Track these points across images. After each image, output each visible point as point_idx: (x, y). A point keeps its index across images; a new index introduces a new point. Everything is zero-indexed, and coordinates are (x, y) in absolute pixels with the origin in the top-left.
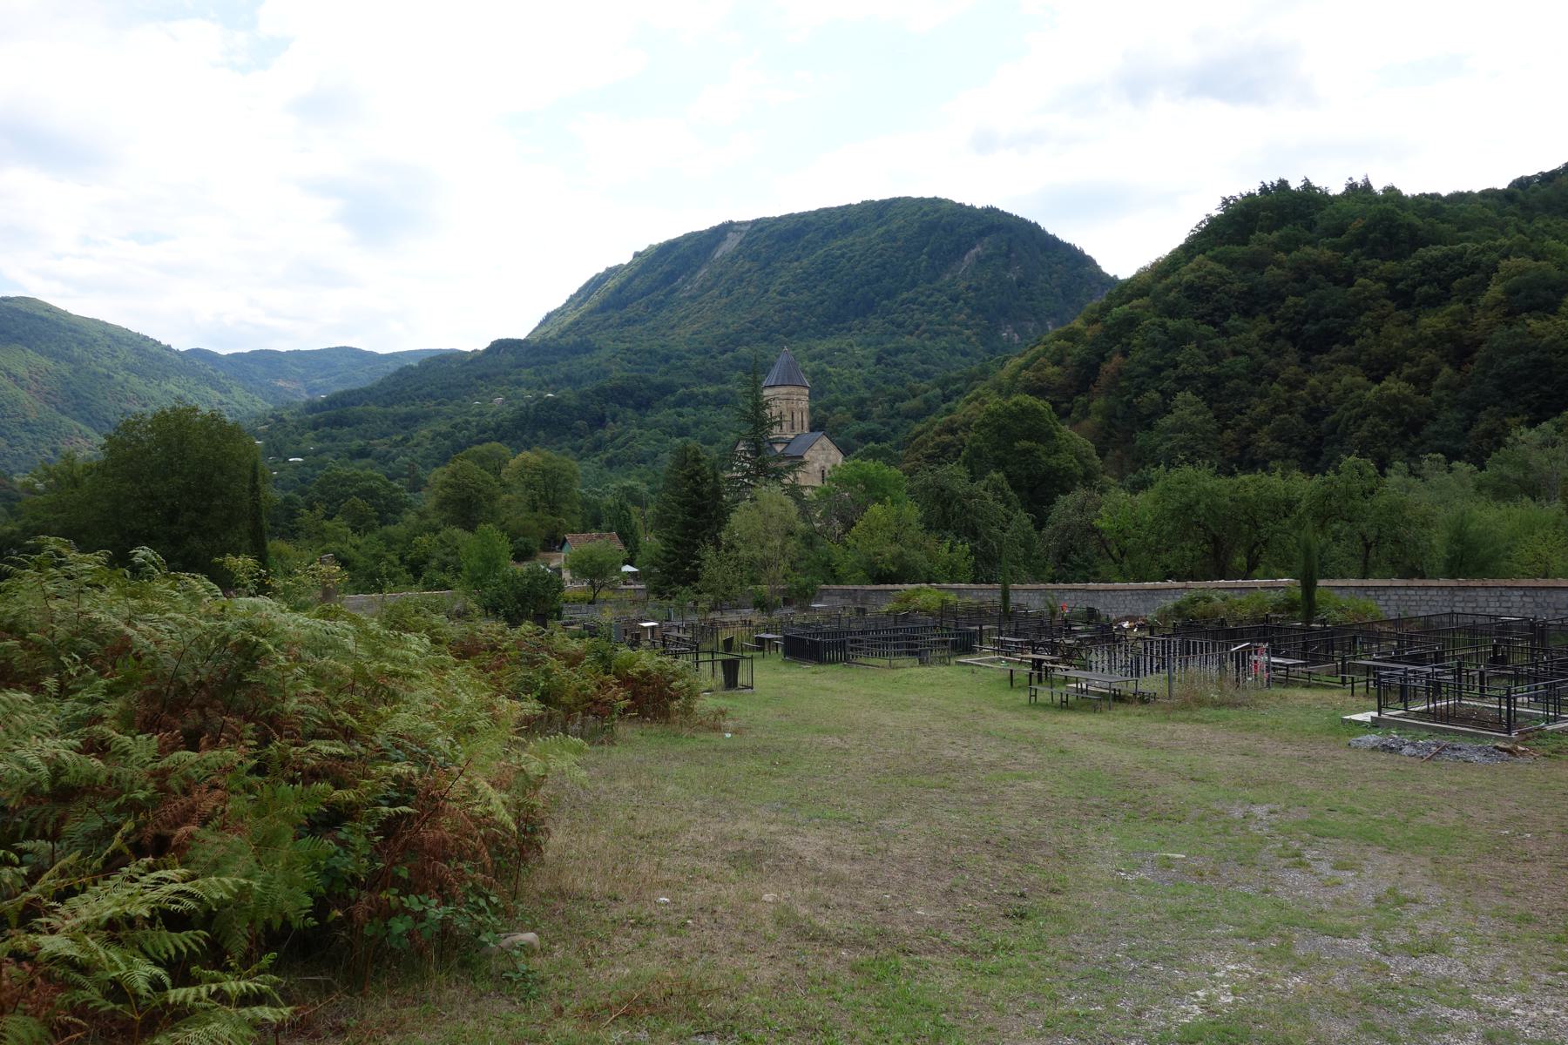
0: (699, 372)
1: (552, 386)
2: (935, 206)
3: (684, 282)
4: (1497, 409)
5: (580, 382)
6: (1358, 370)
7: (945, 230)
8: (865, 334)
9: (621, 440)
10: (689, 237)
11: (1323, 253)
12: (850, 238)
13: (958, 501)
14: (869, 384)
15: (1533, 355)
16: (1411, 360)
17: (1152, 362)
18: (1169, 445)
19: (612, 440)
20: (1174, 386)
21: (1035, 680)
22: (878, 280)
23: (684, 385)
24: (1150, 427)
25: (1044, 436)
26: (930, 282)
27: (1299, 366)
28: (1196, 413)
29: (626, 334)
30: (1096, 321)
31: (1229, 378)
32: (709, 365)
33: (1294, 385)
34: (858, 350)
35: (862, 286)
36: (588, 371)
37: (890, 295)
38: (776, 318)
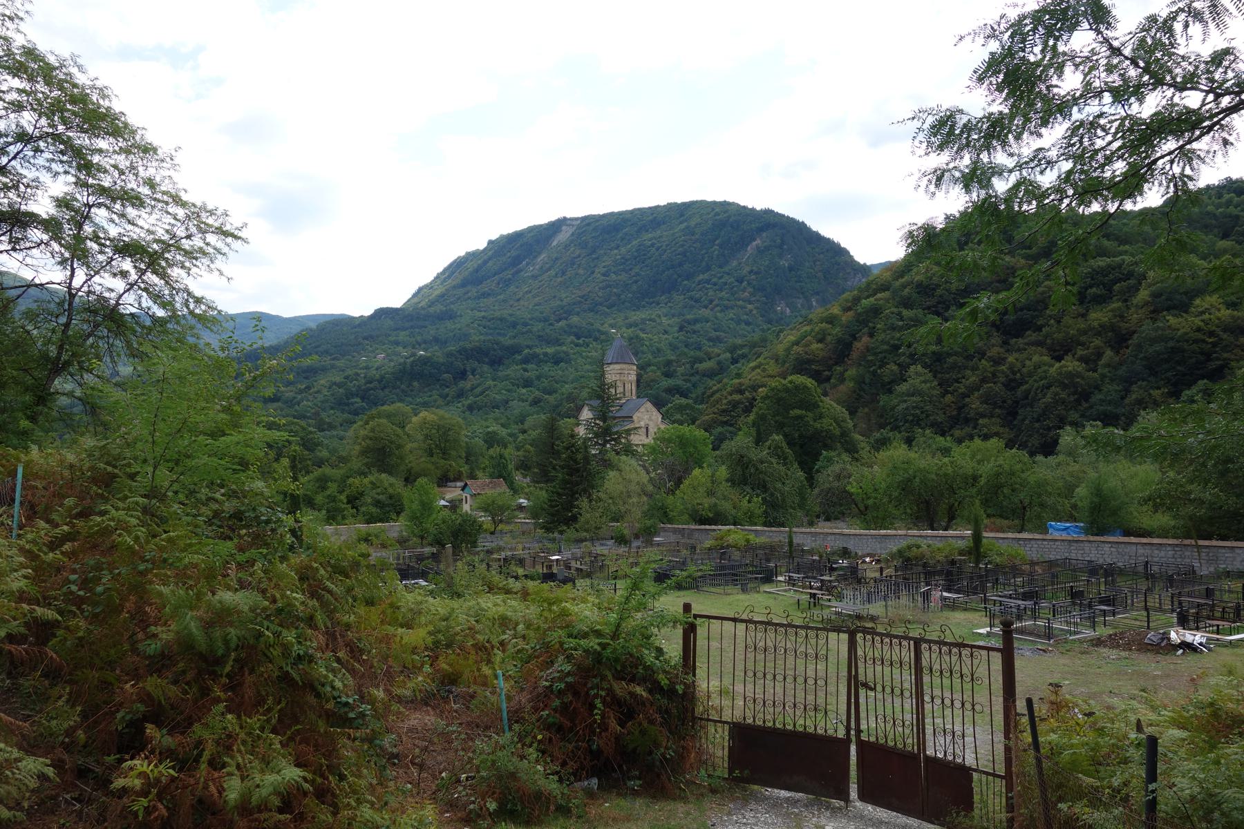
0: (539, 336)
1: (423, 346)
2: (725, 208)
3: (528, 264)
4: (1145, 383)
5: (446, 342)
6: (1044, 351)
7: (732, 227)
8: (671, 307)
9: (479, 389)
10: (531, 229)
11: (1018, 261)
12: (659, 232)
13: (754, 465)
14: (674, 348)
15: (1171, 344)
16: (1083, 344)
17: (892, 342)
18: (905, 406)
19: (472, 389)
20: (908, 360)
21: (812, 604)
22: (680, 265)
23: (528, 347)
24: (890, 391)
25: (810, 405)
26: (720, 267)
27: (1001, 347)
28: (925, 382)
29: (482, 305)
30: (849, 309)
31: (949, 355)
32: (548, 331)
33: (998, 361)
34: (664, 320)
35: (668, 269)
36: (451, 334)
37: (689, 277)
38: (600, 294)
